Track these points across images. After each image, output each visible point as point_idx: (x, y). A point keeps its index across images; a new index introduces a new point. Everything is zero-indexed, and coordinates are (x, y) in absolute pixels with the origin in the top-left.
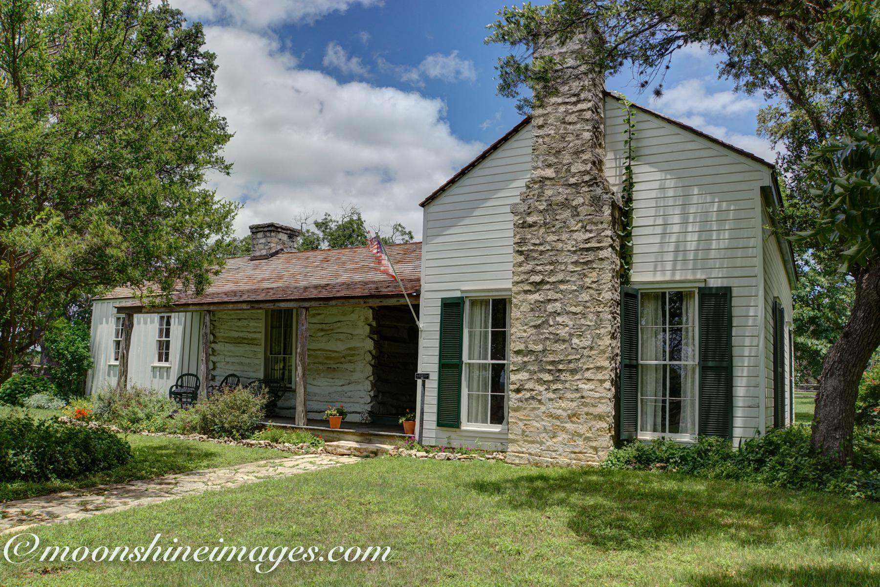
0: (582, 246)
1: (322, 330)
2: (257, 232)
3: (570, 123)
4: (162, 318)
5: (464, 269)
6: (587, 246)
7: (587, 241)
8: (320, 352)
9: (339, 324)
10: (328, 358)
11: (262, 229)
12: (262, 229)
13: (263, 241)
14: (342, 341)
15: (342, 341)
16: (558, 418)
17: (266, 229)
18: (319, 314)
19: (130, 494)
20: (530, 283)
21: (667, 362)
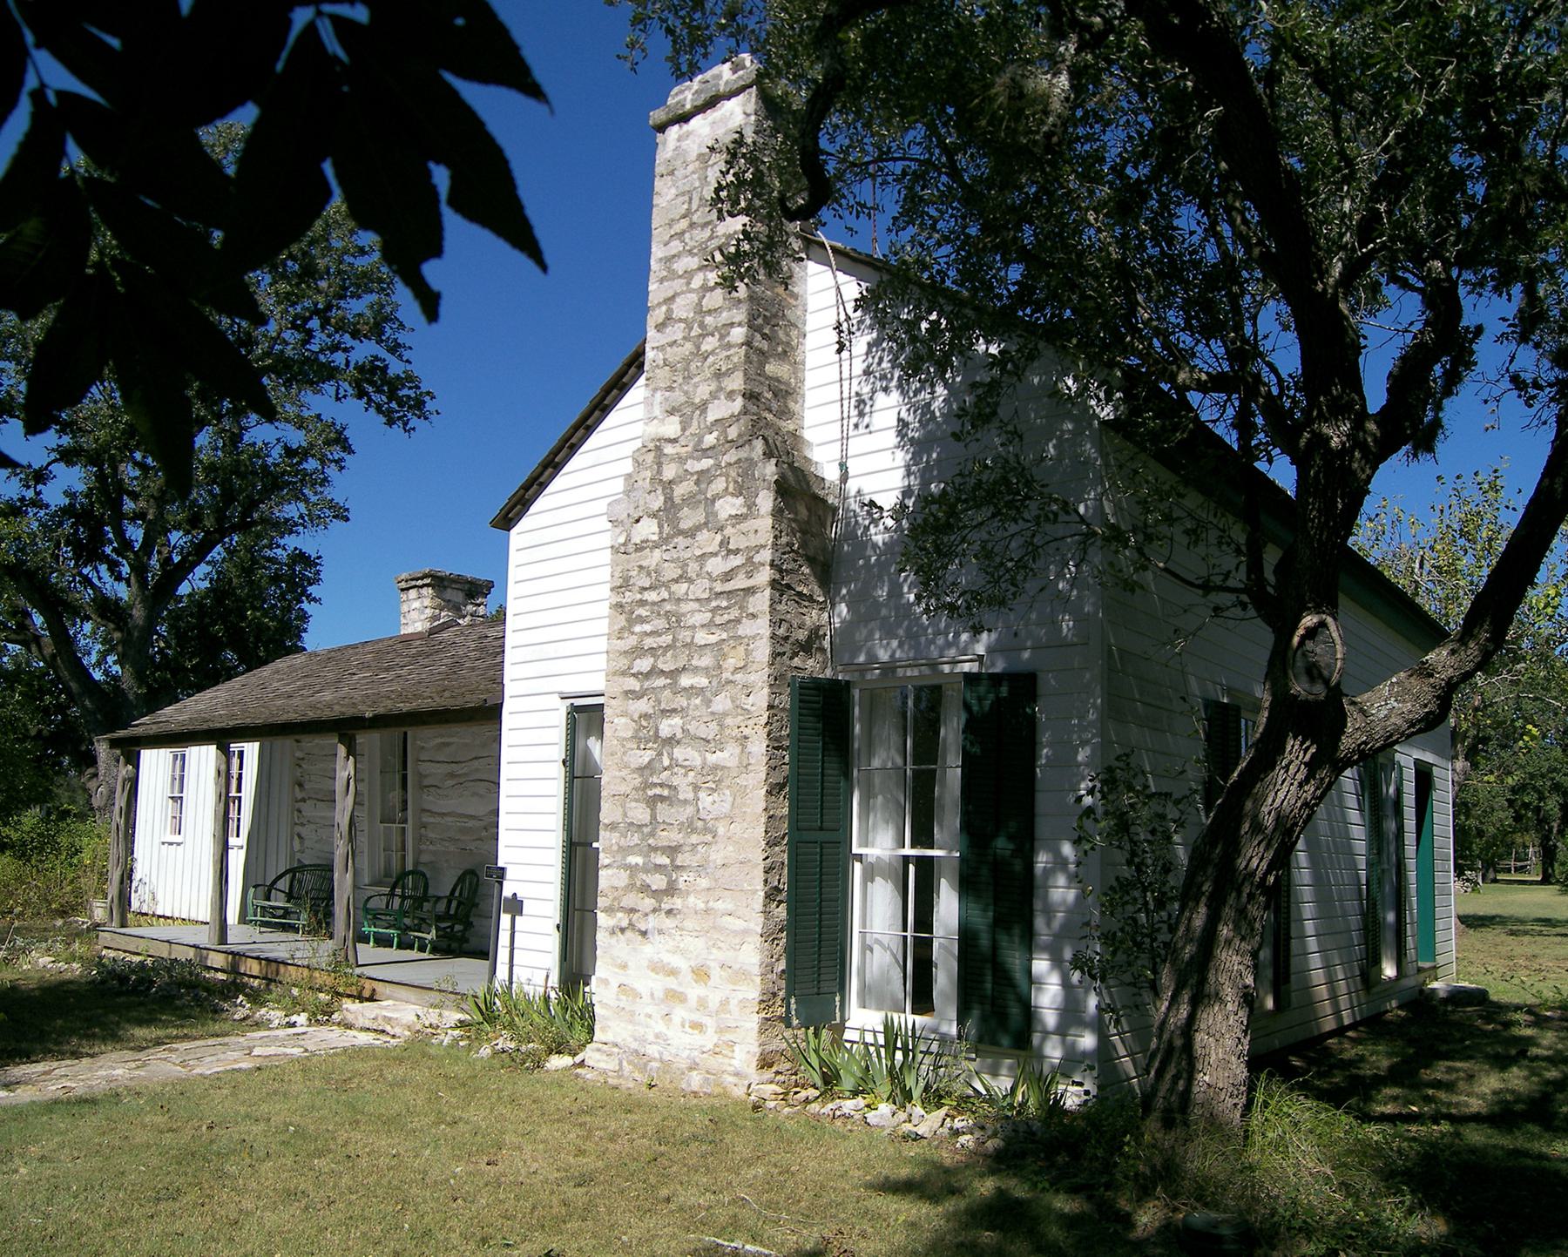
0: (719, 587)
1: (452, 775)
2: (408, 589)
3: (709, 312)
4: (175, 757)
5: (550, 650)
6: (729, 586)
7: (728, 576)
8: (450, 819)
9: (476, 763)
10: (463, 830)
11: (414, 583)
12: (414, 583)
13: (416, 604)
14: (481, 796)
15: (481, 796)
16: (673, 972)
17: (420, 583)
18: (448, 744)
19: (1558, 930)
20: (633, 675)
21: (908, 851)
